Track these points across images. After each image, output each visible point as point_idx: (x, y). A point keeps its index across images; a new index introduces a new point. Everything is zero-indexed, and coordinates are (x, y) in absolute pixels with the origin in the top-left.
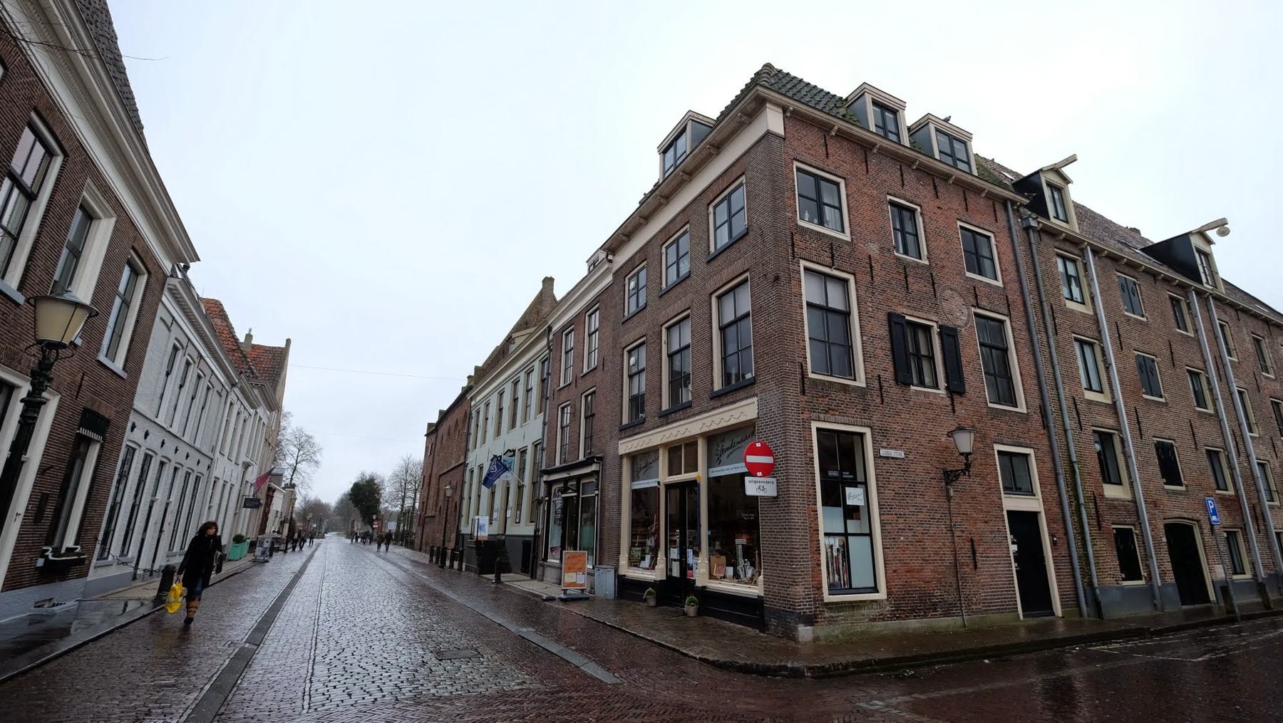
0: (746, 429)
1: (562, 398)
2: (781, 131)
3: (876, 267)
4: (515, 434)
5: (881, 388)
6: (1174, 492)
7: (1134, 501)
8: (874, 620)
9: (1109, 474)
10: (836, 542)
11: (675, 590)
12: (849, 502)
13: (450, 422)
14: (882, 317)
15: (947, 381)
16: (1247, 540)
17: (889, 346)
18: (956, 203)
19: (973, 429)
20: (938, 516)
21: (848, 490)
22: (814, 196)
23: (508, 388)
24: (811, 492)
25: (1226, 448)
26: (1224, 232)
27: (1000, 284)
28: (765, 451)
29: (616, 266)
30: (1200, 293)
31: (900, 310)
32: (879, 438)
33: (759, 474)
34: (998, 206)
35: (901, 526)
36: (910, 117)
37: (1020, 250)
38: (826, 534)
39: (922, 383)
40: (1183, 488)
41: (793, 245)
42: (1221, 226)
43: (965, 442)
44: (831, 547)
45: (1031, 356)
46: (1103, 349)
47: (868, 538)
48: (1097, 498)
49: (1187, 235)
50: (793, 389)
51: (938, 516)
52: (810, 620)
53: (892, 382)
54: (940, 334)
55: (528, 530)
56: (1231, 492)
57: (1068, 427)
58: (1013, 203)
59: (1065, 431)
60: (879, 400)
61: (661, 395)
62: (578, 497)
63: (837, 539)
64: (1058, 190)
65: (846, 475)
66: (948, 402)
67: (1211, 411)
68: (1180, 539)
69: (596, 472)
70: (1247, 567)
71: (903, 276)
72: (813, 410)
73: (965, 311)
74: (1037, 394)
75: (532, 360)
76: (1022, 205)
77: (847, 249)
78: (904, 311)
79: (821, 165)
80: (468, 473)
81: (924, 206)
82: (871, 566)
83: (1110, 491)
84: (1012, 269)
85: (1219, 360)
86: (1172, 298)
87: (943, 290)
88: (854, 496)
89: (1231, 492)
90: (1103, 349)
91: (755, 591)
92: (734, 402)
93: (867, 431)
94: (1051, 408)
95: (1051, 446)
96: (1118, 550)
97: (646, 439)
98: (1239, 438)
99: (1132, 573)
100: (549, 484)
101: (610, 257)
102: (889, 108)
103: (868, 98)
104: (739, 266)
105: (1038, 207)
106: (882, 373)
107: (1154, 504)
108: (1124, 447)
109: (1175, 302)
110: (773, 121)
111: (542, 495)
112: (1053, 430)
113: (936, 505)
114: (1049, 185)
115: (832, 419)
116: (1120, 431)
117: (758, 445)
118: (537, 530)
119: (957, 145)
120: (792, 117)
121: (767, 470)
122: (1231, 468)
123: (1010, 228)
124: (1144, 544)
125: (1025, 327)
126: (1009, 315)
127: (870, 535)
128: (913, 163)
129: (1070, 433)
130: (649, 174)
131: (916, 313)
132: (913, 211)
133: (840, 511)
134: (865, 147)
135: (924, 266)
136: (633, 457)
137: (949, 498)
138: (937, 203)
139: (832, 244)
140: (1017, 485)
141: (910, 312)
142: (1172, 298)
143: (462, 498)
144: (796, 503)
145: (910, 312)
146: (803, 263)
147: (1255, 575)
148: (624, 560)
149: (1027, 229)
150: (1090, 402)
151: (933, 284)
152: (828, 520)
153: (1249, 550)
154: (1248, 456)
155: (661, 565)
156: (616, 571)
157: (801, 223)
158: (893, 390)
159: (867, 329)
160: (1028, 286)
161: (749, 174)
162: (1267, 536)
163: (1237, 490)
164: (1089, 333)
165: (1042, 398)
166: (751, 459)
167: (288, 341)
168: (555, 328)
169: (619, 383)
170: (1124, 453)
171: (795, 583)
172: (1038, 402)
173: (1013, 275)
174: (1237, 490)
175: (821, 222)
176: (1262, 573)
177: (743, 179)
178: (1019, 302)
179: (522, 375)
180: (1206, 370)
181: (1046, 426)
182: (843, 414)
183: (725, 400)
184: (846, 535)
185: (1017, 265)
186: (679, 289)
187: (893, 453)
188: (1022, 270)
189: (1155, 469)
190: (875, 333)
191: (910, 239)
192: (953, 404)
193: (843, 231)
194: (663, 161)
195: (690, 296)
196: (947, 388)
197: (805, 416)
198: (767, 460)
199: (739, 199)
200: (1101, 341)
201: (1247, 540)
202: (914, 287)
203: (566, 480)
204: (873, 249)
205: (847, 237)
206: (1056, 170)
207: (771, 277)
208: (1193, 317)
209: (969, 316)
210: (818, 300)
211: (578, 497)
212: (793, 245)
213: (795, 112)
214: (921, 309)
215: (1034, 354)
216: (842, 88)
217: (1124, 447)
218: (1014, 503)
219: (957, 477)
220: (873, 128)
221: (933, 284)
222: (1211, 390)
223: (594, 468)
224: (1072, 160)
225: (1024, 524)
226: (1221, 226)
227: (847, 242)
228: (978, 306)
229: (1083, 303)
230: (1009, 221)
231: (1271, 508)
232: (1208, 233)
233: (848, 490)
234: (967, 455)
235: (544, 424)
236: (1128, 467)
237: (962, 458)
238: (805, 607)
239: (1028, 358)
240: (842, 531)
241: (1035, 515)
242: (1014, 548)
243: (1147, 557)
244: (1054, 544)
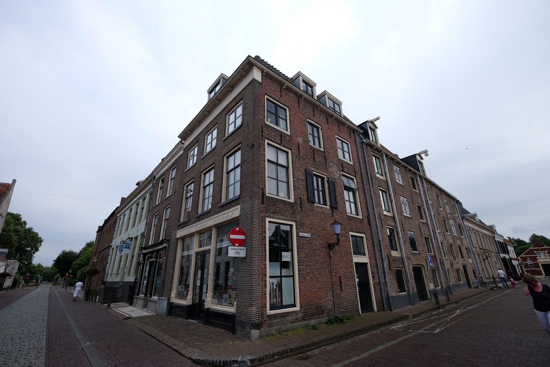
0: (234, 221)
1: (156, 211)
2: (260, 80)
3: (301, 148)
4: (132, 229)
5: (301, 203)
6: (415, 254)
7: (402, 258)
8: (293, 322)
9: (393, 247)
10: (275, 281)
11: (196, 311)
12: (283, 260)
13: (108, 225)
14: (303, 170)
15: (330, 202)
16: (439, 273)
17: (305, 184)
18: (335, 128)
19: (341, 224)
20: (325, 266)
21: (283, 253)
22: (274, 113)
23: (134, 207)
24: (263, 254)
25: (430, 236)
26: (427, 155)
27: (352, 163)
28: (241, 233)
29: (185, 146)
30: (420, 176)
31: (311, 168)
32: (299, 227)
33: (237, 245)
34: (351, 132)
35: (308, 271)
36: (318, 91)
37: (359, 150)
38: (270, 277)
39: (319, 203)
40: (417, 252)
41: (262, 131)
42: (426, 152)
43: (338, 229)
44: (273, 283)
45: (363, 194)
46: (389, 194)
47: (292, 278)
48: (389, 256)
49: (414, 156)
50: (257, 202)
51: (325, 266)
52: (258, 326)
53: (306, 201)
54: (328, 181)
55: (131, 279)
56: (433, 254)
57: (378, 225)
58: (357, 132)
59: (377, 227)
60: (300, 209)
61: (198, 206)
62: (156, 261)
63: (276, 279)
64: (373, 130)
65: (283, 246)
66: (330, 212)
67: (425, 222)
68: (418, 271)
69: (165, 247)
70: (439, 283)
71: (312, 154)
72: (267, 212)
73: (338, 173)
74: (366, 211)
75: (145, 193)
76: (360, 133)
77: (288, 138)
78: (313, 169)
79: (278, 100)
80: (111, 250)
81: (323, 126)
82: (293, 292)
83: (394, 253)
84: (356, 158)
85: (427, 201)
86: (411, 178)
87: (330, 162)
88: (286, 256)
89: (433, 254)
90: (389, 194)
91: (231, 310)
92: (230, 208)
93: (294, 224)
94: (372, 217)
95: (372, 233)
96: (397, 278)
97: (189, 229)
98: (434, 232)
99: (402, 289)
100: (145, 255)
101: (183, 142)
102: (309, 85)
103: (301, 78)
104: (237, 141)
105: (366, 135)
106: (302, 196)
107: (409, 259)
108: (398, 235)
109: (412, 179)
110: (257, 75)
111: (141, 260)
112: (372, 227)
113: (324, 260)
114: (370, 128)
115: (277, 217)
116: (396, 228)
117: (237, 229)
118: (136, 279)
119: (336, 106)
120: (265, 75)
121: (241, 243)
122: (433, 244)
123: (356, 142)
124: (406, 275)
125: (361, 182)
126: (355, 176)
127: (293, 276)
128: (318, 107)
129: (379, 228)
130: (203, 100)
131: (318, 171)
132: (318, 128)
133: (278, 264)
134: (299, 96)
135: (321, 151)
136: (183, 238)
137: (330, 257)
138: (328, 126)
139: (281, 135)
140: (359, 252)
141: (315, 170)
142: (411, 178)
143: (107, 263)
144: (256, 260)
145: (315, 170)
146: (266, 141)
147: (442, 287)
148: (173, 294)
149: (362, 142)
150: (386, 215)
151: (325, 159)
152: (271, 270)
153: (440, 277)
154: (437, 239)
155: (190, 297)
156: (169, 300)
157: (267, 122)
158: (307, 205)
159: (296, 175)
160: (363, 166)
161: (244, 99)
162: (445, 271)
163: (435, 253)
164: (385, 187)
165: (368, 213)
166: (232, 237)
167: (14, 181)
168: (157, 177)
169: (180, 202)
170: (398, 237)
171: (251, 306)
172: (366, 214)
173: (357, 160)
174: (435, 253)
175: (277, 124)
176: (444, 286)
177: (242, 102)
178: (359, 172)
179: (141, 200)
180: (423, 205)
181: (370, 225)
182: (282, 215)
183: (226, 208)
184: (281, 277)
185: (358, 157)
186: (210, 155)
187: (305, 235)
188: (361, 159)
189: (408, 244)
190: (299, 177)
191: (316, 139)
192: (332, 213)
193: (287, 130)
194: (210, 96)
195: (215, 157)
196: (330, 206)
197: (263, 215)
198: (242, 237)
199: (239, 111)
200: (389, 191)
201: (439, 273)
202: (317, 159)
203: (152, 252)
204: (300, 140)
205: (288, 133)
206: (372, 122)
207: (250, 145)
208: (418, 185)
209: (340, 175)
210: (274, 159)
211: (156, 261)
212: (262, 131)
213: (267, 73)
214: (320, 169)
215: (365, 194)
216: (290, 75)
217: (398, 235)
218: (357, 259)
219: (334, 247)
220: (302, 89)
221: (325, 159)
222: (425, 213)
223: (165, 245)
224: (378, 119)
225: (361, 267)
226: (426, 152)
227: (288, 135)
228: (343, 171)
229: (382, 175)
230: (355, 139)
231: (445, 259)
232: (422, 155)
233: (283, 253)
234: (337, 234)
235: (146, 224)
236: (399, 243)
237: (336, 236)
238: (256, 320)
239: (362, 195)
240: (279, 275)
241: (365, 264)
242: (357, 280)
243: (408, 281)
244: (373, 277)
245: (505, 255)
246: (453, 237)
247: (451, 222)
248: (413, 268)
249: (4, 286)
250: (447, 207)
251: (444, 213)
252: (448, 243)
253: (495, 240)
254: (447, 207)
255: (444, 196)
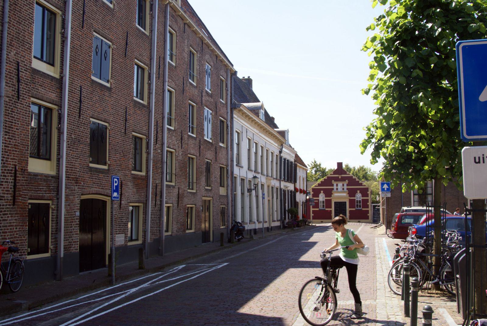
7: (57, 178)
40: (106, 167)
83: (37, 166)
85: (162, 59)
98: (159, 128)
122: (148, 153)
147: (144, 241)
150: (36, 72)
200: (150, 68)
224: (362, 153)
245: (288, 184)
246: (201, 143)
247: (207, 112)
248: (83, 203)
249: (423, 249)
250: (208, 81)
251: (196, 92)
252: (185, 154)
253: (281, 158)
254: (208, 81)
255: (207, 57)
